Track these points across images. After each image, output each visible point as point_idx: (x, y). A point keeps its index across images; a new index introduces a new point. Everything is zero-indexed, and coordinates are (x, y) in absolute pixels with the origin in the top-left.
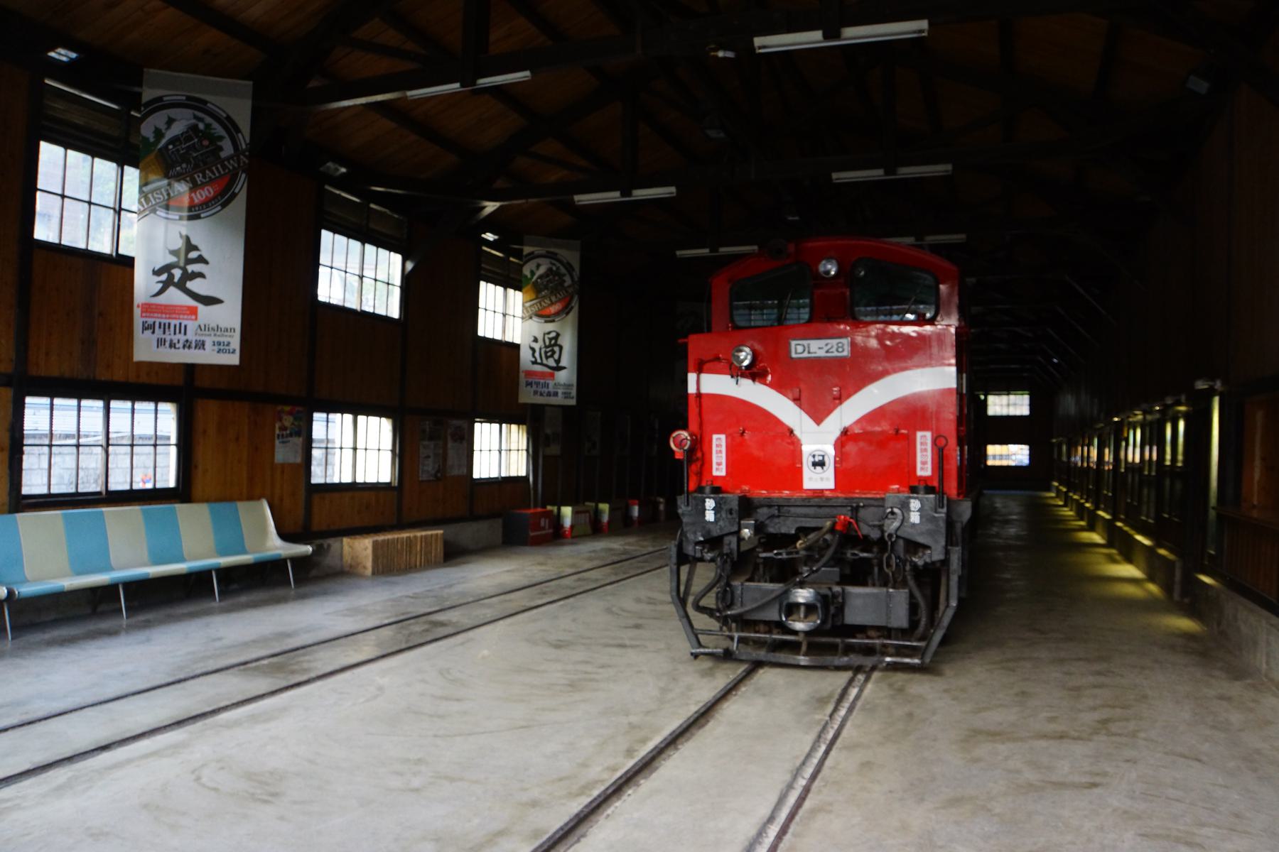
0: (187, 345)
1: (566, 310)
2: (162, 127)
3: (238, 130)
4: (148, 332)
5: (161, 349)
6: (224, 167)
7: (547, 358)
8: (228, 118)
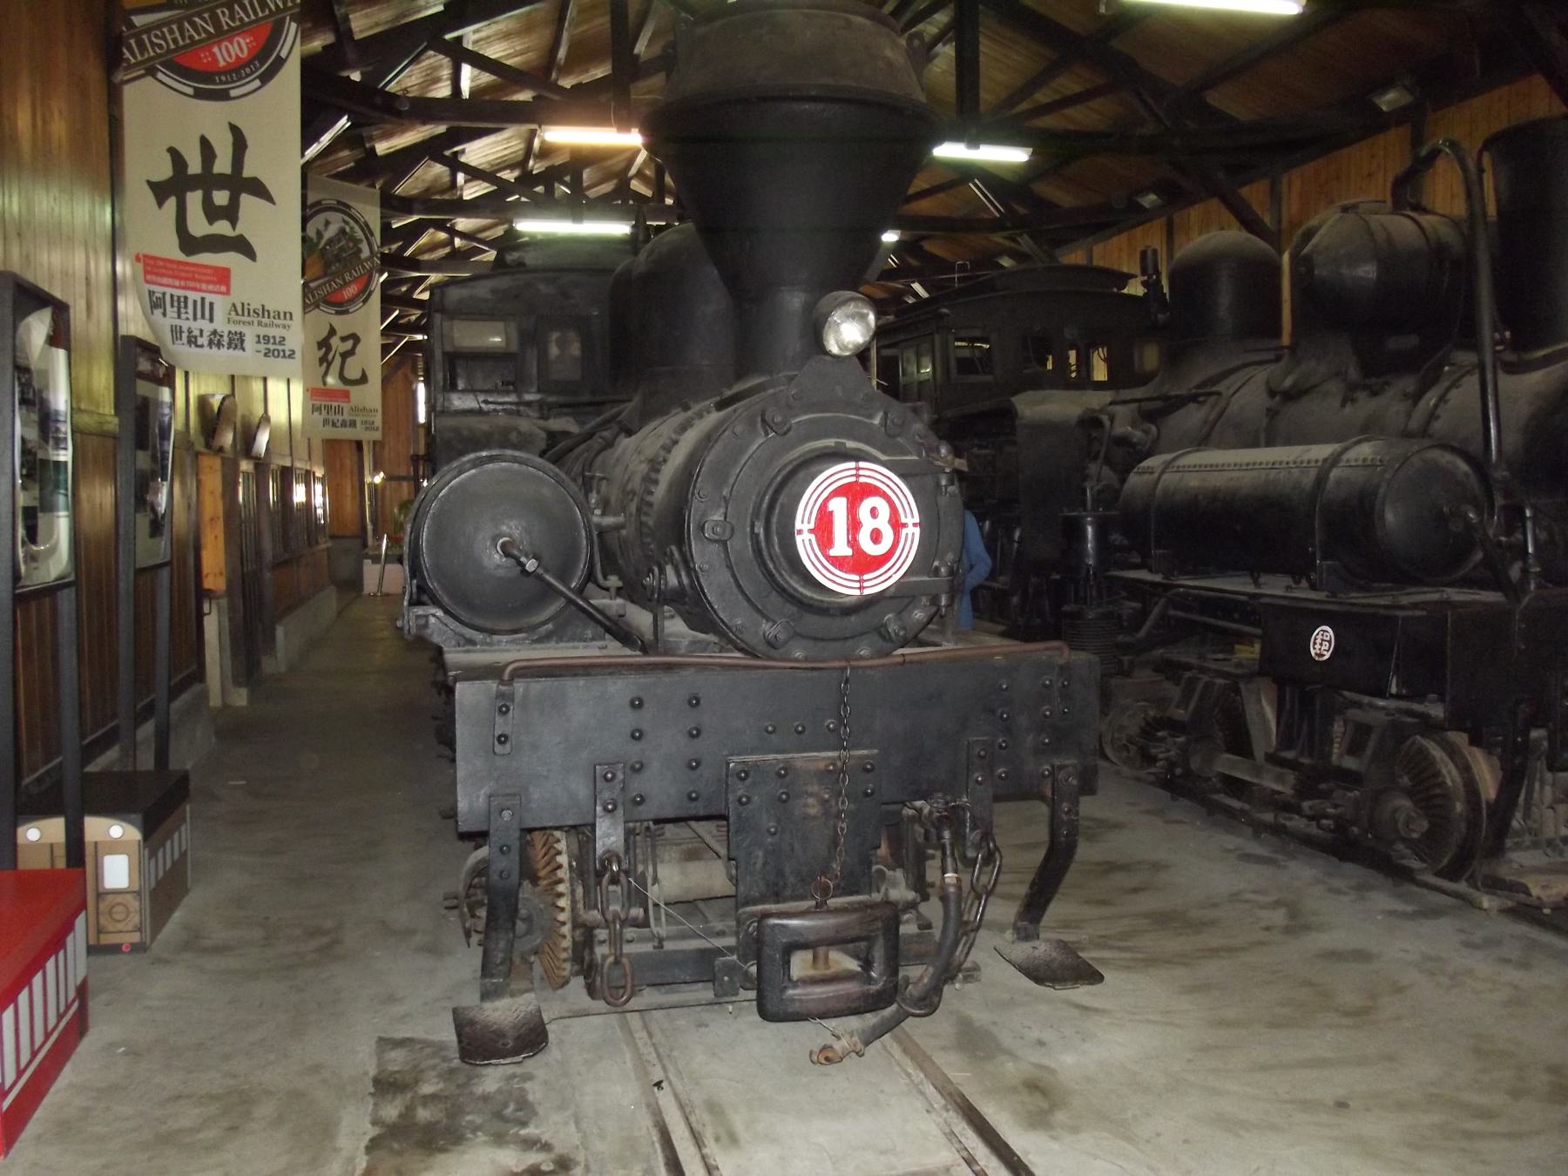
0: (344, 424)
2: (321, 228)
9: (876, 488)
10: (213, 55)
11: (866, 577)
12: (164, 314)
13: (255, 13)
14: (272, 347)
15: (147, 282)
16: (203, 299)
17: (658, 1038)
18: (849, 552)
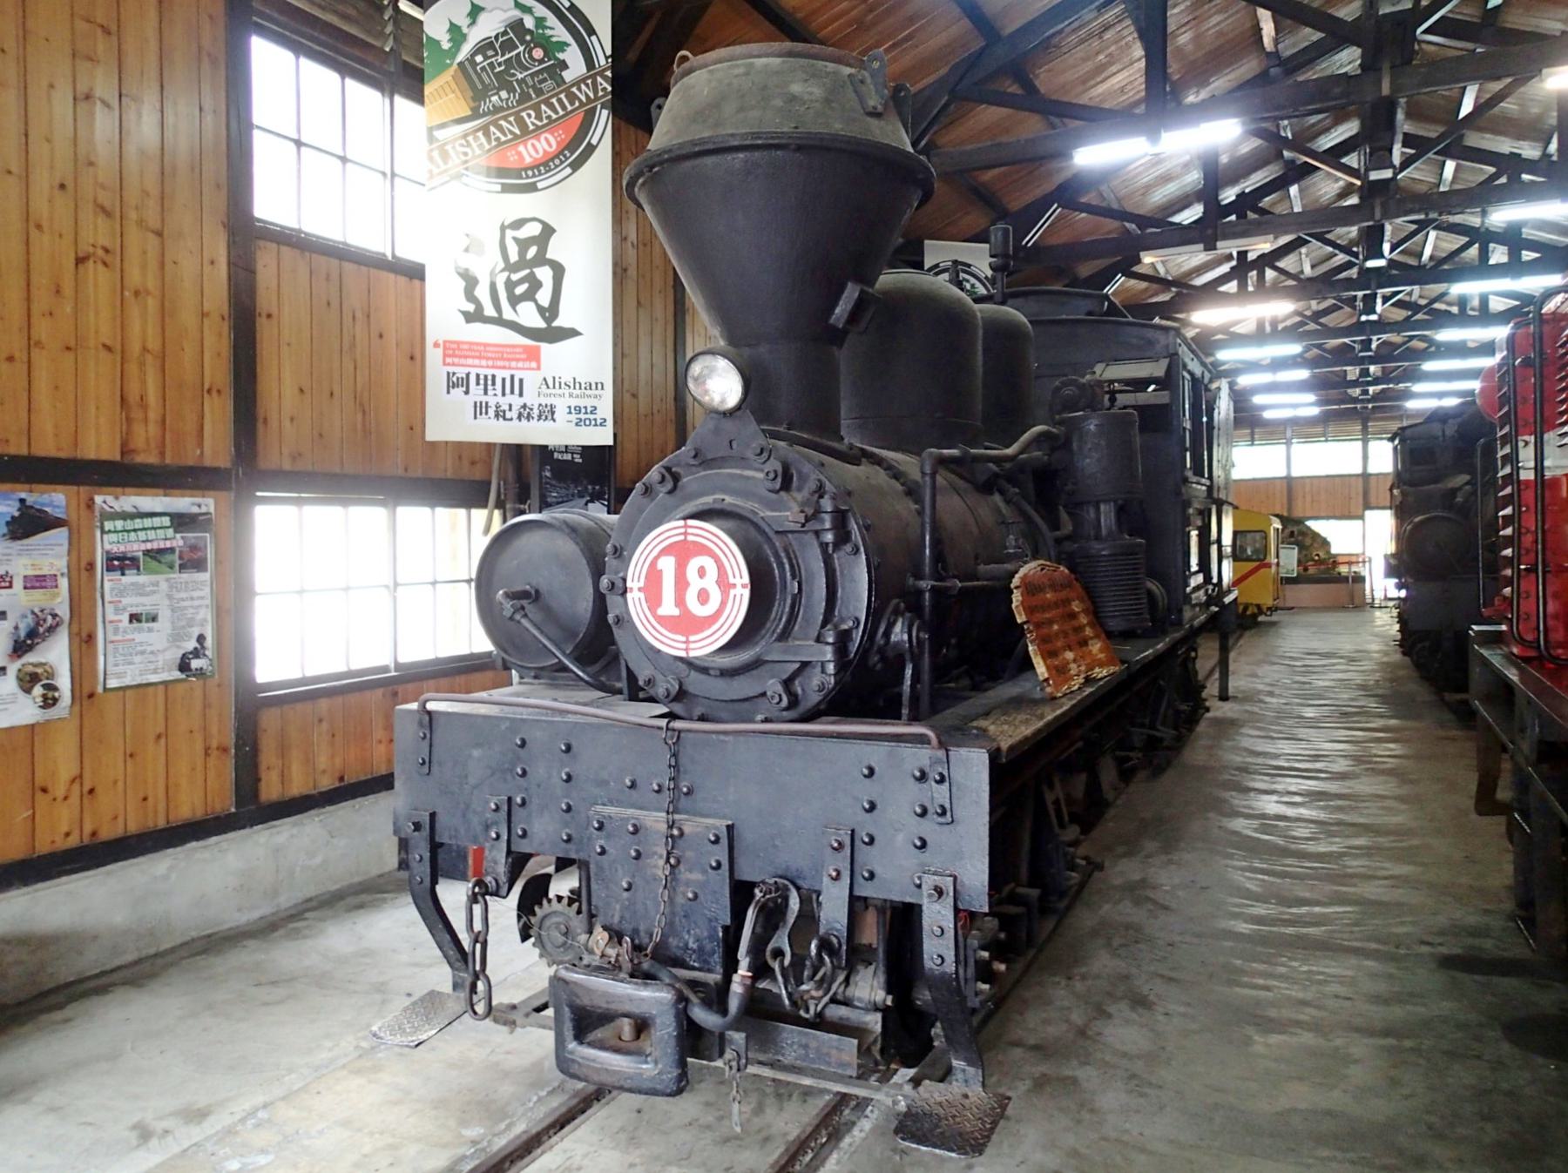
1: (576, 152)
2: (463, 22)
3: (591, 31)
4: (458, 392)
5: (482, 420)
6: (572, 98)
7: (514, 301)
8: (573, 8)
9: (704, 546)
10: (519, 154)
11: (692, 638)
12: (467, 392)
13: (564, 108)
14: (582, 416)
15: (445, 364)
16: (512, 377)
17: (397, 1049)
18: (676, 612)
